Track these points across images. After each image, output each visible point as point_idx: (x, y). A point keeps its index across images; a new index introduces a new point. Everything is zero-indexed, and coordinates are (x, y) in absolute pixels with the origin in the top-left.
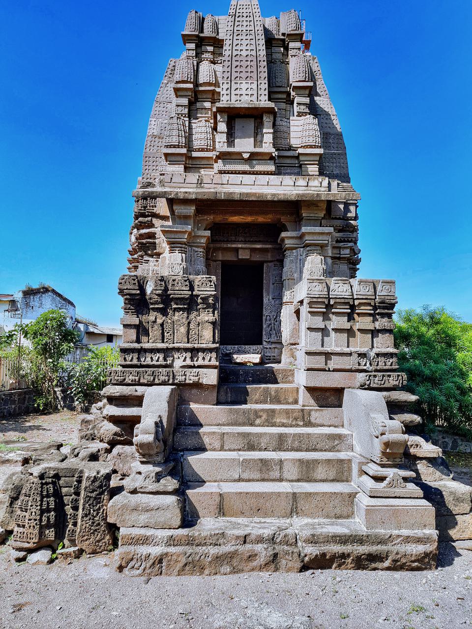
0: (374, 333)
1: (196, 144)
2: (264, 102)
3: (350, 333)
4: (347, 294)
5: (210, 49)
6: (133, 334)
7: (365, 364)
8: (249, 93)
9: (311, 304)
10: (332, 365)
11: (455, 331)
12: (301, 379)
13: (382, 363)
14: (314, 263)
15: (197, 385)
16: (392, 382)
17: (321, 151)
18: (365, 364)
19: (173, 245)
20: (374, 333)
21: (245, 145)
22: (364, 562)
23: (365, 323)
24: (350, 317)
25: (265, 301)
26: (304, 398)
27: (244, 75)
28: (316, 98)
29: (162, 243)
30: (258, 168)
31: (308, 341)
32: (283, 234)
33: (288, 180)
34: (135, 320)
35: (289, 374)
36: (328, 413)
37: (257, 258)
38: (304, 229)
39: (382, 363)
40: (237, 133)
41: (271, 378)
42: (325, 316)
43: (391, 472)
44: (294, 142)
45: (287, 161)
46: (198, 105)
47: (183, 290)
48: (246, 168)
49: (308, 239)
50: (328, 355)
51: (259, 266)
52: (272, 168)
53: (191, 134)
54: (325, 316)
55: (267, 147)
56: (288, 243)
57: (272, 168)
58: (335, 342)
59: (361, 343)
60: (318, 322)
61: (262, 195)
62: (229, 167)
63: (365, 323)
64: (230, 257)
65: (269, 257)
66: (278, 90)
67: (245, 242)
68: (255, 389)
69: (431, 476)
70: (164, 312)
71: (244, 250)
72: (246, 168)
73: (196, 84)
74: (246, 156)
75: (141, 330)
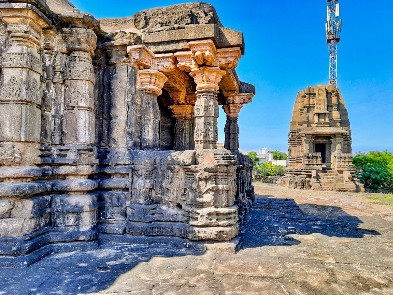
0: (349, 162)
1: (310, 119)
2: (327, 112)
3: (345, 162)
4: (344, 156)
5: (312, 95)
6: (307, 162)
7: (347, 167)
8: (323, 109)
9: (338, 157)
10: (341, 167)
11: (387, 157)
12: (336, 169)
13: (350, 167)
14: (339, 146)
15: (319, 170)
16: (352, 169)
17: (340, 120)
18: (347, 167)
19: (306, 143)
20: (349, 162)
21: (322, 121)
22: (345, 191)
23: (348, 160)
24: (345, 159)
25: (326, 153)
26: (337, 172)
27: (321, 104)
28: (339, 100)
29: (304, 142)
30: (325, 125)
31: (337, 163)
32: (331, 139)
33: (332, 128)
34: (308, 160)
35: (334, 168)
36: (341, 175)
37: (324, 143)
38: (336, 139)
39: (350, 167)
40: (320, 117)
41: (331, 169)
42: (340, 159)
43: (349, 181)
44: (333, 118)
45: (332, 123)
46: (310, 109)
47: (146, 78)
48: (323, 125)
49: (337, 141)
50: (341, 165)
51: (325, 144)
52: (329, 125)
53: (308, 116)
54: (340, 159)
55: (327, 121)
56: (332, 141)
57: (329, 125)
58: (342, 163)
59: (347, 163)
60: (339, 160)
61: (326, 132)
62: (318, 126)
63: (348, 160)
64: (318, 143)
65: (327, 142)
66: (330, 105)
67: (321, 139)
68: (328, 171)
69: (357, 183)
70: (312, 159)
71: (321, 141)
72: (323, 125)
73: (309, 105)
74: (322, 123)
75: (309, 161)
